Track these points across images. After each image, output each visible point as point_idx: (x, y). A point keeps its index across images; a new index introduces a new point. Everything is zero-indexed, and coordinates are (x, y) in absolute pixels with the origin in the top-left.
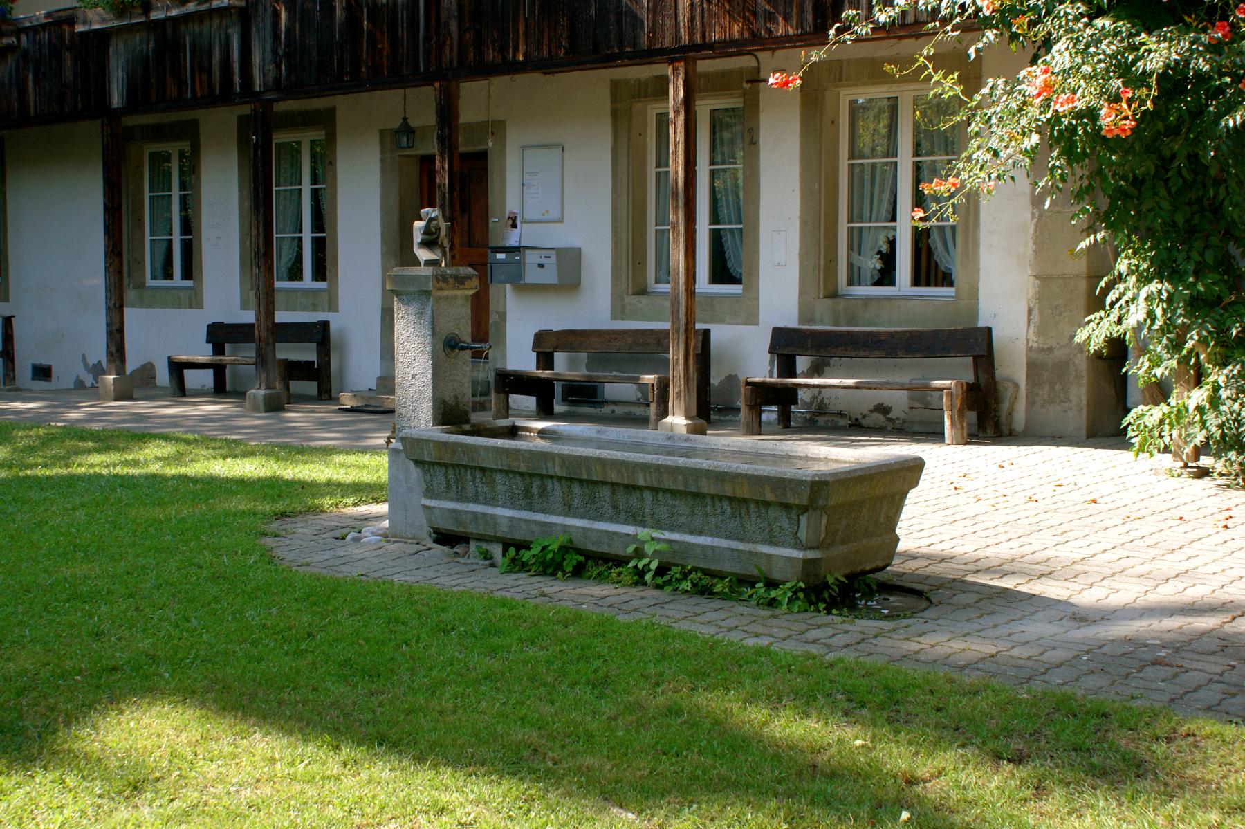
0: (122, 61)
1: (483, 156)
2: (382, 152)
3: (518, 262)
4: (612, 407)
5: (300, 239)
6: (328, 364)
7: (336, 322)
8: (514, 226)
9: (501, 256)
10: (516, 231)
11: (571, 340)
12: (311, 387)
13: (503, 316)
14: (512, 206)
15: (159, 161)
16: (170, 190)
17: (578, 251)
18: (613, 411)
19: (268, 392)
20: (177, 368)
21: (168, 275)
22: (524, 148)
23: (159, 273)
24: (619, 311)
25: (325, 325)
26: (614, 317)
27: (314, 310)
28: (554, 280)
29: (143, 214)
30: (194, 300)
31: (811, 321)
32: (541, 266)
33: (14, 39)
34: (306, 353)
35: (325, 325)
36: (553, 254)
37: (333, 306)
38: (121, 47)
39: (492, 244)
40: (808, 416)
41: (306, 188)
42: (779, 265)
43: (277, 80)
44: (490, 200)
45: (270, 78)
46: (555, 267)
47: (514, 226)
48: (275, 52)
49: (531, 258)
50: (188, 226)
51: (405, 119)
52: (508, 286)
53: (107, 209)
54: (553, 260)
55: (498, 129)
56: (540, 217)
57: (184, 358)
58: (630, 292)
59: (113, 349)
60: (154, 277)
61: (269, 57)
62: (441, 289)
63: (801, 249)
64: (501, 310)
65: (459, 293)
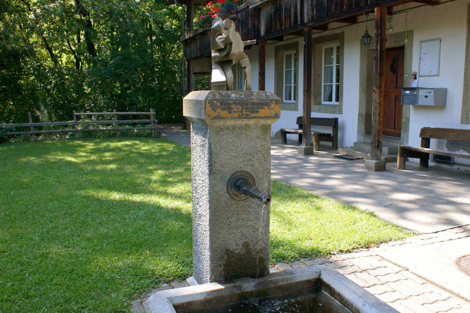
0: (264, 18)
1: (402, 48)
2: (361, 49)
3: (415, 95)
7: (341, 118)
8: (415, 78)
9: (408, 92)
10: (416, 81)
11: (439, 133)
12: (330, 144)
13: (408, 119)
14: (415, 69)
15: (289, 57)
17: (446, 90)
18: (459, 168)
19: (306, 147)
20: (284, 133)
21: (330, 100)
22: (421, 42)
23: (288, 98)
25: (336, 120)
26: (462, 122)
27: (334, 113)
28: (432, 104)
29: (283, 77)
32: (426, 97)
33: (236, 15)
34: (328, 130)
35: (336, 120)
36: (432, 91)
37: (341, 112)
38: (264, 13)
39: (405, 86)
41: (334, 65)
43: (312, 17)
44: (405, 67)
45: (310, 17)
46: (433, 98)
47: (415, 78)
48: (312, 5)
49: (422, 93)
51: (367, 31)
52: (411, 106)
54: (432, 94)
55: (409, 34)
56: (428, 74)
57: (288, 130)
61: (310, 7)
62: (219, 118)
64: (407, 116)
65: (251, 122)
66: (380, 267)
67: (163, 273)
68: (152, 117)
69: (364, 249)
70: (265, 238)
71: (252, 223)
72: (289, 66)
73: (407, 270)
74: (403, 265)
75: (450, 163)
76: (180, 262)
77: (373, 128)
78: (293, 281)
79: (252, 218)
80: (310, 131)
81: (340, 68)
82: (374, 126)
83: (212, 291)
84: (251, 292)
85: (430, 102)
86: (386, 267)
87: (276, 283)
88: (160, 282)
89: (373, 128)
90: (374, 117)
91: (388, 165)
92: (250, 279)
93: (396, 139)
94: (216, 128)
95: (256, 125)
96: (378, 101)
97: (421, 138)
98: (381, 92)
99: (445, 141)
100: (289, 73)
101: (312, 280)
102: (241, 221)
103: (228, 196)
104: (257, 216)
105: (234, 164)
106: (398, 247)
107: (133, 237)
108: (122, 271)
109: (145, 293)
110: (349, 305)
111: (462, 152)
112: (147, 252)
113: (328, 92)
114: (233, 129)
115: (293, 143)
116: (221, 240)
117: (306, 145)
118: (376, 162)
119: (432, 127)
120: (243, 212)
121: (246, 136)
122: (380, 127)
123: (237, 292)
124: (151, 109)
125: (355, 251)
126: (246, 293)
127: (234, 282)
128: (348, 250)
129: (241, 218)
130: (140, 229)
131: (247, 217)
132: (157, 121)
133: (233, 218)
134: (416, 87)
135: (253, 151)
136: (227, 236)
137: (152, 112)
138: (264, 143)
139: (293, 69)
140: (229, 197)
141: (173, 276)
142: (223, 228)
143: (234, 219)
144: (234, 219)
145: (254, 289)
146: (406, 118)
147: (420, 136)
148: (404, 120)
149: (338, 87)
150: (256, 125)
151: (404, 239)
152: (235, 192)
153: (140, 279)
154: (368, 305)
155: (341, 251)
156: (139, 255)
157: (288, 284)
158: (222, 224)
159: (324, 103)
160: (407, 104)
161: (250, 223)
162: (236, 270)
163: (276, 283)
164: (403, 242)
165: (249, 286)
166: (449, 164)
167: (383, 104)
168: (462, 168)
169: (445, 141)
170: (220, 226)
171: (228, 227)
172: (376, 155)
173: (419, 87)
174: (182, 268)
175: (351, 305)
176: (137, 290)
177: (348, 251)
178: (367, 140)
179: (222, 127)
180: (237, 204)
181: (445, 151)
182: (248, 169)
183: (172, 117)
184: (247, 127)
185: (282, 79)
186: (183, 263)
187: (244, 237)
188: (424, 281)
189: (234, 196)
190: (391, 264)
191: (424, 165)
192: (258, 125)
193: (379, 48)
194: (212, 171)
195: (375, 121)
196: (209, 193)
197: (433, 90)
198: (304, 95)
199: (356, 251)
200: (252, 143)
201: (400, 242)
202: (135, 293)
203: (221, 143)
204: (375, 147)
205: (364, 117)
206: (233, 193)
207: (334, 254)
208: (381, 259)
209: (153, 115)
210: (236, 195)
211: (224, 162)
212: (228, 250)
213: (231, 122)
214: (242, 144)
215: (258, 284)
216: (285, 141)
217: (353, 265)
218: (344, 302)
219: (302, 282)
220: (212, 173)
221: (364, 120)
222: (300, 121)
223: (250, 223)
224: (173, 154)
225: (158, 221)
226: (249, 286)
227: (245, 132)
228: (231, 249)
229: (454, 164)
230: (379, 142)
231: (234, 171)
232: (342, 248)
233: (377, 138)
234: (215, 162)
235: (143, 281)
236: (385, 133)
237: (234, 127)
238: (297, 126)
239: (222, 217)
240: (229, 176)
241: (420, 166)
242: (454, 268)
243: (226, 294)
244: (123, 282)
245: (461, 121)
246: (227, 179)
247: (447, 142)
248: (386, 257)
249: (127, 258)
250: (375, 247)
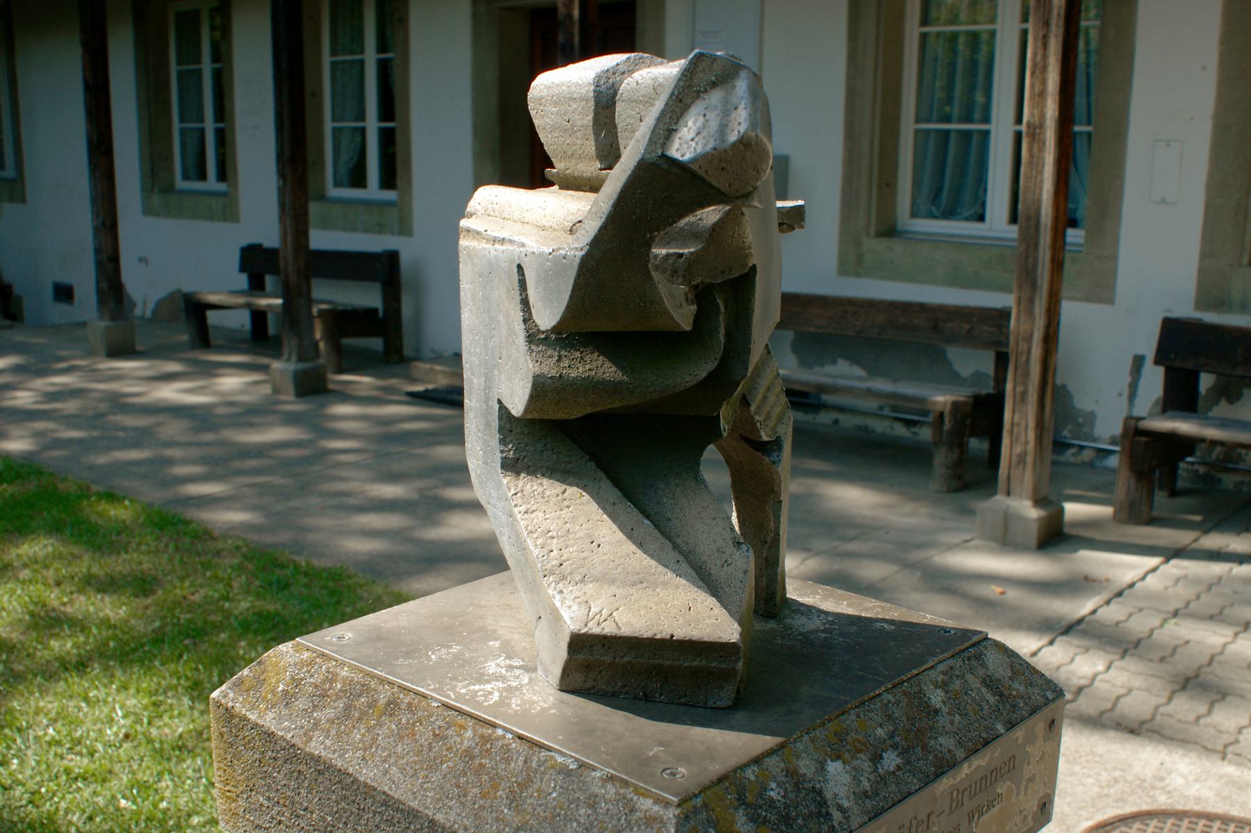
4: (834, 415)
5: (363, 130)
6: (398, 311)
7: (408, 250)
12: (376, 343)
16: (199, 62)
18: (836, 422)
19: (302, 366)
21: (202, 176)
24: (852, 263)
25: (392, 257)
26: (843, 270)
30: (228, 211)
31: (1221, 304)
34: (367, 297)
35: (392, 257)
37: (405, 228)
40: (1202, 470)
41: (371, 57)
42: (1164, 201)
50: (390, 106)
53: (88, 88)
57: (213, 298)
58: (872, 231)
59: (105, 285)
60: (186, 177)
63: (1211, 176)
72: (189, 52)
80: (310, 302)
81: (396, 72)
100: (191, 82)
113: (347, 155)
115: (233, 343)
117: (301, 359)
139: (207, 66)
149: (388, 138)
159: (334, 192)
168: (848, 421)
185: (167, 103)
193: (576, 13)
198: (281, 174)
216: (203, 337)
222: (256, 263)
238: (242, 281)
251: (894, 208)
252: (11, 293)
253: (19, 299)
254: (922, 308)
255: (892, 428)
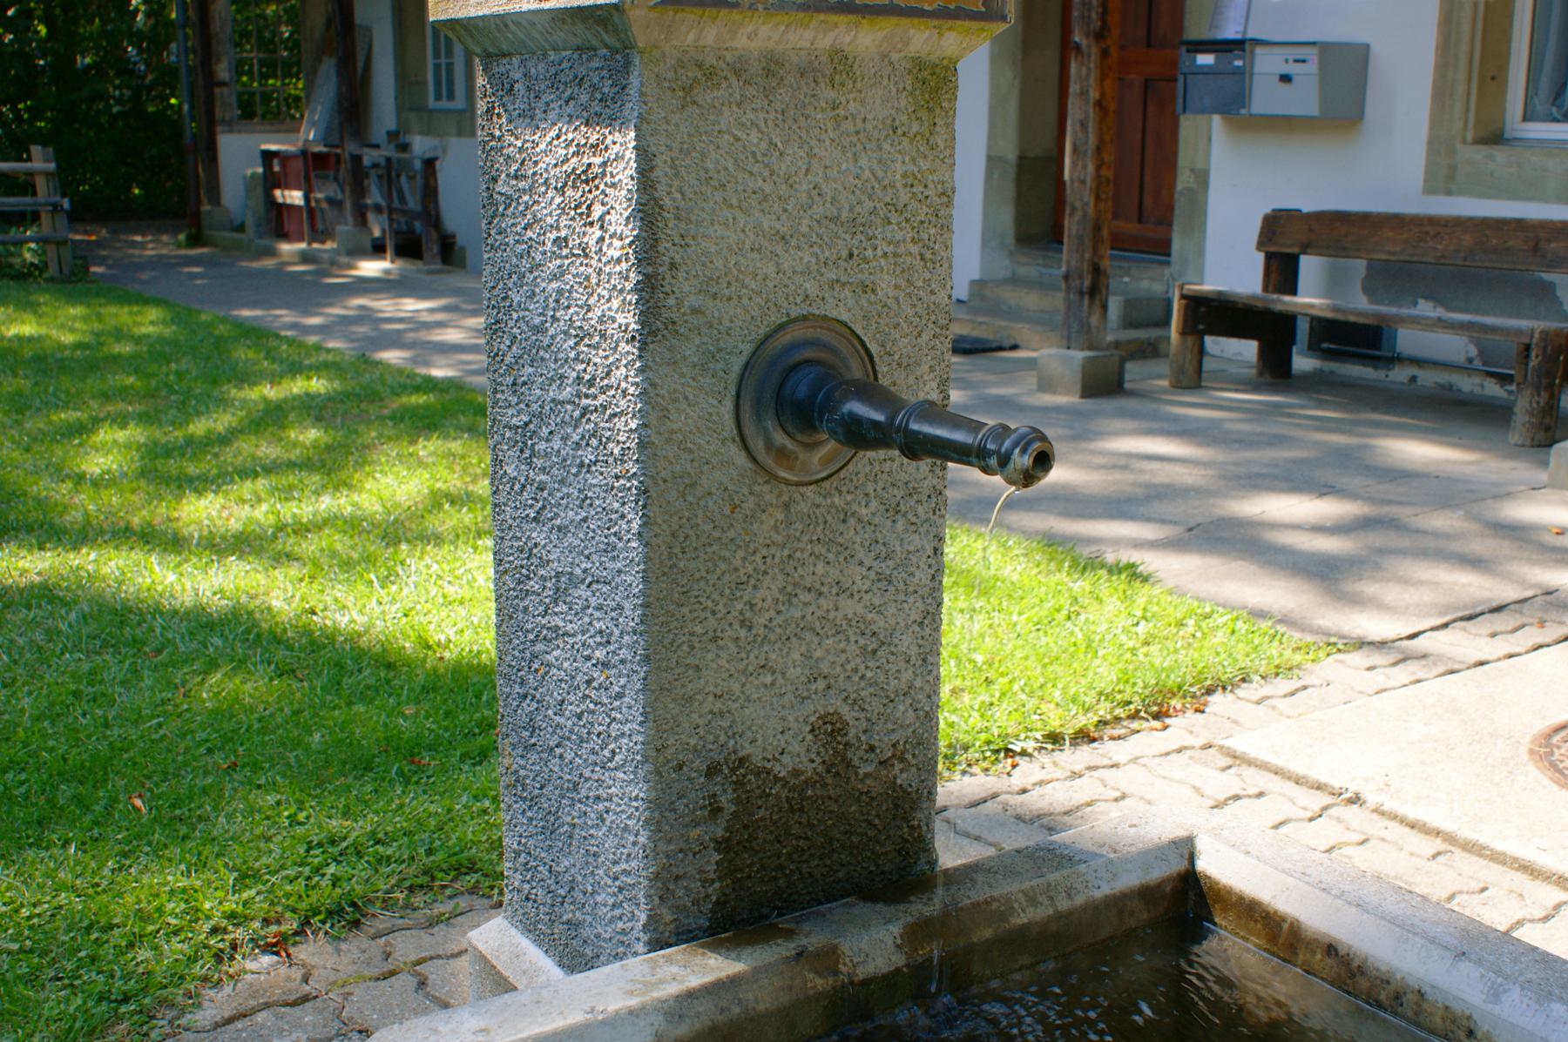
3: (1240, 72)
9: (1205, 59)
11: (1336, 232)
13: (1203, 178)
18: (1413, 379)
24: (1441, 178)
32: (1285, 79)
36: (1312, 54)
39: (1193, 32)
49: (1267, 64)
52: (1216, 119)
54: (1312, 68)
58: (1470, 136)
64: (1200, 165)
66: (1236, 797)
67: (245, 904)
68: (40, 183)
69: (1145, 724)
70: (918, 683)
71: (860, 609)
73: (1356, 800)
74: (1336, 784)
75: (1378, 358)
76: (315, 840)
77: (1074, 209)
78: (1079, 900)
79: (856, 576)
82: (1077, 204)
83: (691, 995)
84: (886, 976)
85: (1303, 99)
86: (1261, 795)
87: (1002, 917)
88: (234, 947)
89: (1074, 209)
90: (1074, 164)
91: (1133, 370)
92: (864, 909)
93: (1153, 262)
94: (681, 64)
95: (884, 56)
96: (1094, 94)
97: (1261, 257)
98: (1105, 54)
99: (1359, 266)
101: (1160, 885)
102: (805, 597)
103: (740, 458)
104: (886, 567)
105: (769, 278)
106: (1282, 704)
107: (45, 736)
108: (25, 912)
109: (170, 1014)
110: (1398, 996)
111: (1425, 308)
112: (138, 802)
114: (768, 73)
116: (707, 707)
118: (1086, 359)
119: (1305, 210)
120: (819, 549)
121: (837, 121)
122: (1102, 206)
123: (820, 983)
124: (36, 150)
125: (1109, 731)
126: (865, 983)
127: (789, 934)
128: (1081, 731)
129: (808, 581)
130: (76, 694)
131: (834, 573)
132: (66, 204)
133: (767, 581)
134: (1239, 37)
135: (869, 205)
136: (736, 686)
137: (40, 161)
138: (922, 163)
140: (750, 465)
141: (294, 911)
142: (715, 639)
143: (770, 589)
144: (770, 589)
145: (899, 960)
146: (1192, 170)
147: (1261, 245)
148: (1184, 181)
150: (884, 56)
151: (1296, 671)
152: (780, 438)
153: (131, 945)
154: (1516, 990)
155: (1055, 738)
156: (96, 823)
157: (1059, 916)
158: (712, 622)
160: (1203, 111)
161: (849, 607)
162: (780, 867)
163: (1002, 917)
164: (1300, 684)
165: (873, 945)
166: (1375, 361)
167: (1112, 106)
169: (1359, 266)
170: (699, 630)
171: (743, 632)
172: (1085, 328)
173: (1250, 35)
174: (332, 869)
175: (1410, 998)
176: (126, 999)
177: (1084, 737)
178: (1022, 271)
179: (711, 60)
180: (787, 506)
181: (1359, 304)
182: (844, 308)
183: (129, 190)
184: (841, 65)
186: (333, 842)
187: (821, 684)
188: (1438, 844)
189: (770, 462)
190: (1276, 778)
191: (1275, 369)
192: (895, 57)
194: (657, 316)
195: (1083, 182)
196: (642, 445)
197: (1314, 51)
199: (1116, 732)
200: (864, 162)
201: (1283, 685)
202: (119, 1019)
203: (703, 156)
204: (1081, 293)
205: (1012, 175)
206: (769, 444)
207: (1024, 753)
208: (1229, 761)
209: (47, 174)
210: (782, 455)
211: (719, 263)
212: (742, 761)
213: (764, 31)
214: (815, 163)
215: (917, 933)
217: (1123, 797)
218: (1364, 984)
219: (1118, 902)
220: (655, 326)
221: (1010, 187)
223: (849, 607)
224: (159, 352)
225: (160, 652)
226: (873, 945)
227: (832, 94)
228: (756, 754)
229: (1395, 359)
230: (1097, 271)
231: (775, 318)
232: (1054, 724)
233: (1087, 256)
234: (673, 266)
235: (144, 954)
236: (1118, 242)
237: (772, 65)
239: (713, 578)
240: (747, 348)
241: (1261, 374)
242: (1535, 777)
243: (764, 998)
244: (39, 968)
245: (1426, 180)
246: (738, 363)
247: (1369, 267)
248: (1253, 752)
249: (37, 844)
250: (1190, 714)
251: (1503, 110)
252: (453, 244)
253: (463, 249)
254: (1520, 225)
255: (1482, 387)
